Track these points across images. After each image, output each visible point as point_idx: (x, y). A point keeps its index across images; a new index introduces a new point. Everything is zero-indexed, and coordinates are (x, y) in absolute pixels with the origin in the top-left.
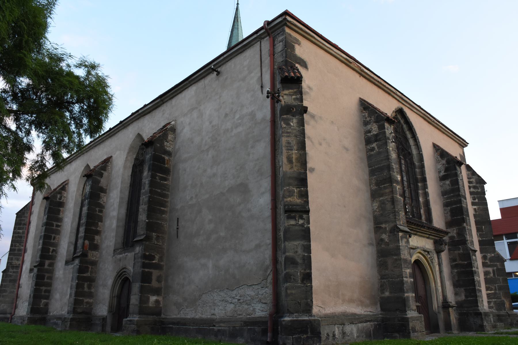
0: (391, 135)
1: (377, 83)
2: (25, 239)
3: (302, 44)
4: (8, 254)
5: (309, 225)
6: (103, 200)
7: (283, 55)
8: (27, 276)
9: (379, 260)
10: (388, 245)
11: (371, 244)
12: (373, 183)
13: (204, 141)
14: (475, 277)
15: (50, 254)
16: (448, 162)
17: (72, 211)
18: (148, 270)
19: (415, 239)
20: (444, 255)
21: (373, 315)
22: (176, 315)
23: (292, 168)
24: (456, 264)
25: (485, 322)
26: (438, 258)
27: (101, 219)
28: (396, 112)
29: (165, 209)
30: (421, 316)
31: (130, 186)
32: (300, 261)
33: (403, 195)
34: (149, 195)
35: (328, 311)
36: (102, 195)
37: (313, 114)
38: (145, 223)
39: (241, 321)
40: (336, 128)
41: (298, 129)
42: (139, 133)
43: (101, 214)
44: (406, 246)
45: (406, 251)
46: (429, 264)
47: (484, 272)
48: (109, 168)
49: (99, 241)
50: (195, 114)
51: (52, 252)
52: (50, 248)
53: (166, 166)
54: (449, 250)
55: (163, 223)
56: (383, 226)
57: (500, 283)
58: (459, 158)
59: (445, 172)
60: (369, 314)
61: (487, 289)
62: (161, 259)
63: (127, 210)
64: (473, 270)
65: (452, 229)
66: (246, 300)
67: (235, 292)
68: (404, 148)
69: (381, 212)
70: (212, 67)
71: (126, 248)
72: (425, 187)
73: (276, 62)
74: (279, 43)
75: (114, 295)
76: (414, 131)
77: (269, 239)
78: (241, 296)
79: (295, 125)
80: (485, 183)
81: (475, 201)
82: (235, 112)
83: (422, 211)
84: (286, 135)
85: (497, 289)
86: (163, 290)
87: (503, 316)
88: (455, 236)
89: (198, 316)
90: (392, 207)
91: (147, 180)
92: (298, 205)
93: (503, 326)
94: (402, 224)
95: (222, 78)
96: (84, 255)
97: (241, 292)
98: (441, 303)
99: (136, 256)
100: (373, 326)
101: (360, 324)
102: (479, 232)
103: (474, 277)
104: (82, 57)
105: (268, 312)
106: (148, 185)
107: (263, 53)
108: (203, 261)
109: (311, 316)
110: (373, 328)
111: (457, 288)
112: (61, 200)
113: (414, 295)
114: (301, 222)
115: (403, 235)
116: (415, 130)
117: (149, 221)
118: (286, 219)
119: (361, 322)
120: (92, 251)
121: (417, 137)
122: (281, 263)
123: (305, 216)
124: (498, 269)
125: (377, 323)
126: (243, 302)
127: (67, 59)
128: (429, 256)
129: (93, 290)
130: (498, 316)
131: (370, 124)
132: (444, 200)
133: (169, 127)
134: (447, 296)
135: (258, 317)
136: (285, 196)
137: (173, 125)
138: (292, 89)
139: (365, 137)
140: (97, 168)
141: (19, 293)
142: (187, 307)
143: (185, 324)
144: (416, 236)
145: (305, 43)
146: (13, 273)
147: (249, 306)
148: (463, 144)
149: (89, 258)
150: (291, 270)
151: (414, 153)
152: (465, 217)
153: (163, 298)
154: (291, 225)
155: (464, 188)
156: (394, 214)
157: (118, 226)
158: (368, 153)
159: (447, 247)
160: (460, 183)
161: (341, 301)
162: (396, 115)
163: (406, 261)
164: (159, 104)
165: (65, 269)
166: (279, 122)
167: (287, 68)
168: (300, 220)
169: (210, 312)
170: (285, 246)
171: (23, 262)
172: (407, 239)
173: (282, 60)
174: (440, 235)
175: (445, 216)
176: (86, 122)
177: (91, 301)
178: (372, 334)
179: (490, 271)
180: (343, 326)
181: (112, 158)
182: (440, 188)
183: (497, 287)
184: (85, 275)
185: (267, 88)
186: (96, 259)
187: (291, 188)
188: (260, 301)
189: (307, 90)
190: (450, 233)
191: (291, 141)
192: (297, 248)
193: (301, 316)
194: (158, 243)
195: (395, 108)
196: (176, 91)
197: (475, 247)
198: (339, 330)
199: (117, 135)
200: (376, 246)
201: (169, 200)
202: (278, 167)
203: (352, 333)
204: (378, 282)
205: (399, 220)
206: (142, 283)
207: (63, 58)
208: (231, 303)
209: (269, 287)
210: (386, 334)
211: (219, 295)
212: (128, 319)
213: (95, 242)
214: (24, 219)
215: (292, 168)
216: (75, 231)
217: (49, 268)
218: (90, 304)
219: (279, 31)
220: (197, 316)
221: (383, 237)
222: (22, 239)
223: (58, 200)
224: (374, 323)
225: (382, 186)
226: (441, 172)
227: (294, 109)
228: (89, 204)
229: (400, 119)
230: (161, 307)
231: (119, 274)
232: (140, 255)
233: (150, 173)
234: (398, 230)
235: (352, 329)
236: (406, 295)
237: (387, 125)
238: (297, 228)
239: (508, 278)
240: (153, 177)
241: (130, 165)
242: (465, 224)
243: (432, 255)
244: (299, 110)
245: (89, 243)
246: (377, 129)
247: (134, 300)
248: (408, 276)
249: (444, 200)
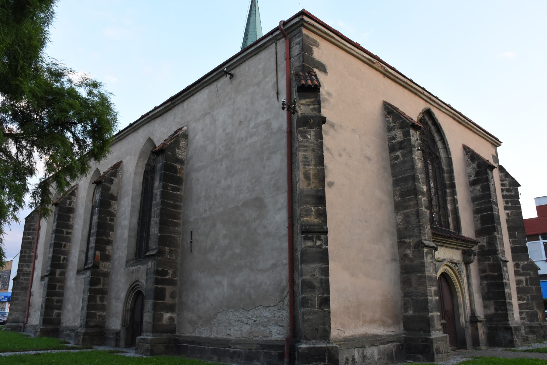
0: (417, 142)
1: (402, 83)
2: (35, 245)
3: (320, 46)
4: (19, 256)
5: (327, 247)
6: (113, 208)
7: (299, 59)
8: (38, 284)
9: (403, 276)
10: (412, 261)
11: (394, 260)
12: (397, 195)
13: (217, 150)
14: (505, 289)
15: (61, 262)
16: (479, 166)
17: (82, 218)
18: (162, 286)
19: (442, 250)
20: (473, 267)
21: (396, 335)
22: (191, 333)
23: (309, 184)
24: (486, 275)
25: (516, 337)
26: (467, 270)
27: (112, 228)
28: (423, 113)
29: (178, 221)
30: (446, 336)
31: (142, 193)
32: (317, 284)
33: (430, 206)
34: (161, 207)
35: (348, 334)
36: (112, 203)
37: (333, 123)
38: (157, 236)
39: (257, 344)
40: (357, 136)
41: (316, 143)
42: (149, 138)
43: (112, 223)
44: (431, 262)
45: (431, 267)
46: (457, 276)
47: (516, 281)
48: (120, 173)
49: (111, 252)
50: (208, 120)
51: (63, 261)
53: (178, 175)
54: (479, 260)
55: (176, 236)
56: (407, 240)
57: (533, 293)
58: (491, 161)
59: (475, 177)
60: (392, 334)
61: (519, 299)
62: (174, 274)
63: (139, 219)
64: (503, 282)
65: (482, 238)
66: (262, 322)
67: (251, 313)
68: (432, 152)
69: (405, 226)
70: (225, 70)
71: (138, 260)
72: (454, 193)
73: (292, 66)
74: (296, 45)
75: (127, 309)
76: (442, 133)
77: (285, 259)
78: (257, 318)
79: (312, 138)
80: (519, 185)
81: (508, 205)
82: (250, 120)
83: (450, 219)
84: (303, 150)
85: (530, 299)
86: (177, 306)
87: (535, 327)
88: (486, 245)
89: (213, 335)
90: (417, 220)
91: (159, 191)
92: (315, 225)
93: (535, 338)
94: (427, 239)
95: (235, 82)
96: (96, 266)
97: (257, 312)
98: (468, 317)
99: (148, 271)
100: (396, 347)
101: (381, 346)
102: (512, 238)
103: (504, 289)
104: (83, 74)
105: (285, 336)
106: (160, 197)
107: (278, 56)
108: (218, 278)
109: (329, 343)
110: (395, 349)
111: (486, 300)
112: (70, 205)
113: (439, 314)
114: (319, 243)
115: (428, 250)
116: (443, 132)
117: (161, 235)
118: (302, 240)
119: (382, 344)
120: (103, 262)
121: (446, 139)
122: (298, 285)
123: (323, 237)
124: (531, 278)
125: (399, 343)
126: (259, 324)
127: (68, 74)
128: (457, 268)
129: (105, 303)
130: (530, 327)
131: (394, 131)
132: (474, 207)
133: (180, 133)
134: (475, 310)
135: (275, 340)
136: (302, 216)
137: (185, 131)
138: (309, 98)
139: (388, 144)
140: (107, 174)
142: (202, 326)
143: (200, 344)
144: (443, 248)
145: (323, 44)
147: (265, 328)
148: (495, 143)
149: (101, 269)
150: (307, 295)
151: (443, 157)
152: (496, 225)
153: (178, 315)
154: (308, 246)
155: (496, 194)
156: (418, 228)
157: (129, 236)
158: (392, 162)
159: (476, 257)
160: (492, 188)
161: (361, 323)
162: (423, 116)
163: (430, 278)
164: (170, 107)
165: (76, 279)
166: (296, 134)
167: (305, 74)
168: (317, 241)
169: (225, 332)
170: (302, 269)
172: (433, 255)
173: (299, 65)
174: (469, 245)
175: (475, 224)
176: (90, 143)
177: (104, 314)
178: (394, 356)
179: (522, 280)
180: (363, 349)
181: (122, 163)
182: (470, 194)
183: (529, 297)
184: (97, 287)
185: (283, 98)
186: (107, 270)
187: (309, 207)
188: (277, 324)
189: (326, 97)
190: (480, 242)
191: (308, 156)
192: (314, 271)
193: (318, 342)
194: (171, 257)
195: (422, 109)
196: (188, 94)
197: (506, 258)
198: (359, 354)
199: (127, 138)
200: (400, 261)
201: (182, 211)
202: (295, 182)
203: (373, 356)
204: (401, 300)
205: (424, 234)
206: (155, 299)
207: (64, 73)
208: (247, 324)
209: (286, 309)
210: (408, 354)
211: (235, 315)
212: (141, 337)
213: (107, 253)
214: (33, 224)
215: (309, 184)
216: (86, 239)
217: (60, 277)
218: (103, 318)
219: (295, 32)
220: (212, 335)
221: (407, 253)
222: (32, 245)
223: (67, 206)
224: (396, 344)
225: (407, 198)
226: (471, 176)
227: (312, 120)
228: (100, 212)
229: (427, 120)
230: (175, 324)
231: (132, 287)
232: (152, 270)
233: (161, 184)
234: (423, 246)
235: (373, 352)
236: (430, 314)
237: (412, 131)
238: (314, 249)
239: (540, 281)
240: (165, 187)
241: (141, 171)
242: (496, 233)
243: (460, 267)
244: (316, 122)
245: (101, 254)
246: (402, 136)
247: (147, 317)
248: (433, 294)
249: (474, 207)
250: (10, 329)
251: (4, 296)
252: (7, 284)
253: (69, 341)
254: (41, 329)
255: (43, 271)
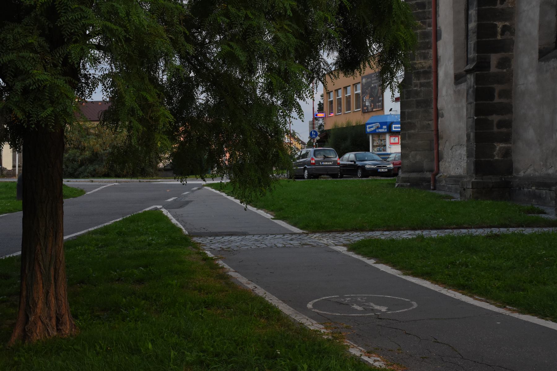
2: (432, 10)
8: (451, 92)
15: (499, 37)
47: (512, 112)
51: (503, 33)
52: (496, 24)
141: (439, 127)
146: (420, 87)
171: (437, 60)
217: (500, 70)
250: (409, 184)
251: (380, 123)
252: (381, 99)
253: (541, 208)
254: (473, 183)
255: (456, 62)
